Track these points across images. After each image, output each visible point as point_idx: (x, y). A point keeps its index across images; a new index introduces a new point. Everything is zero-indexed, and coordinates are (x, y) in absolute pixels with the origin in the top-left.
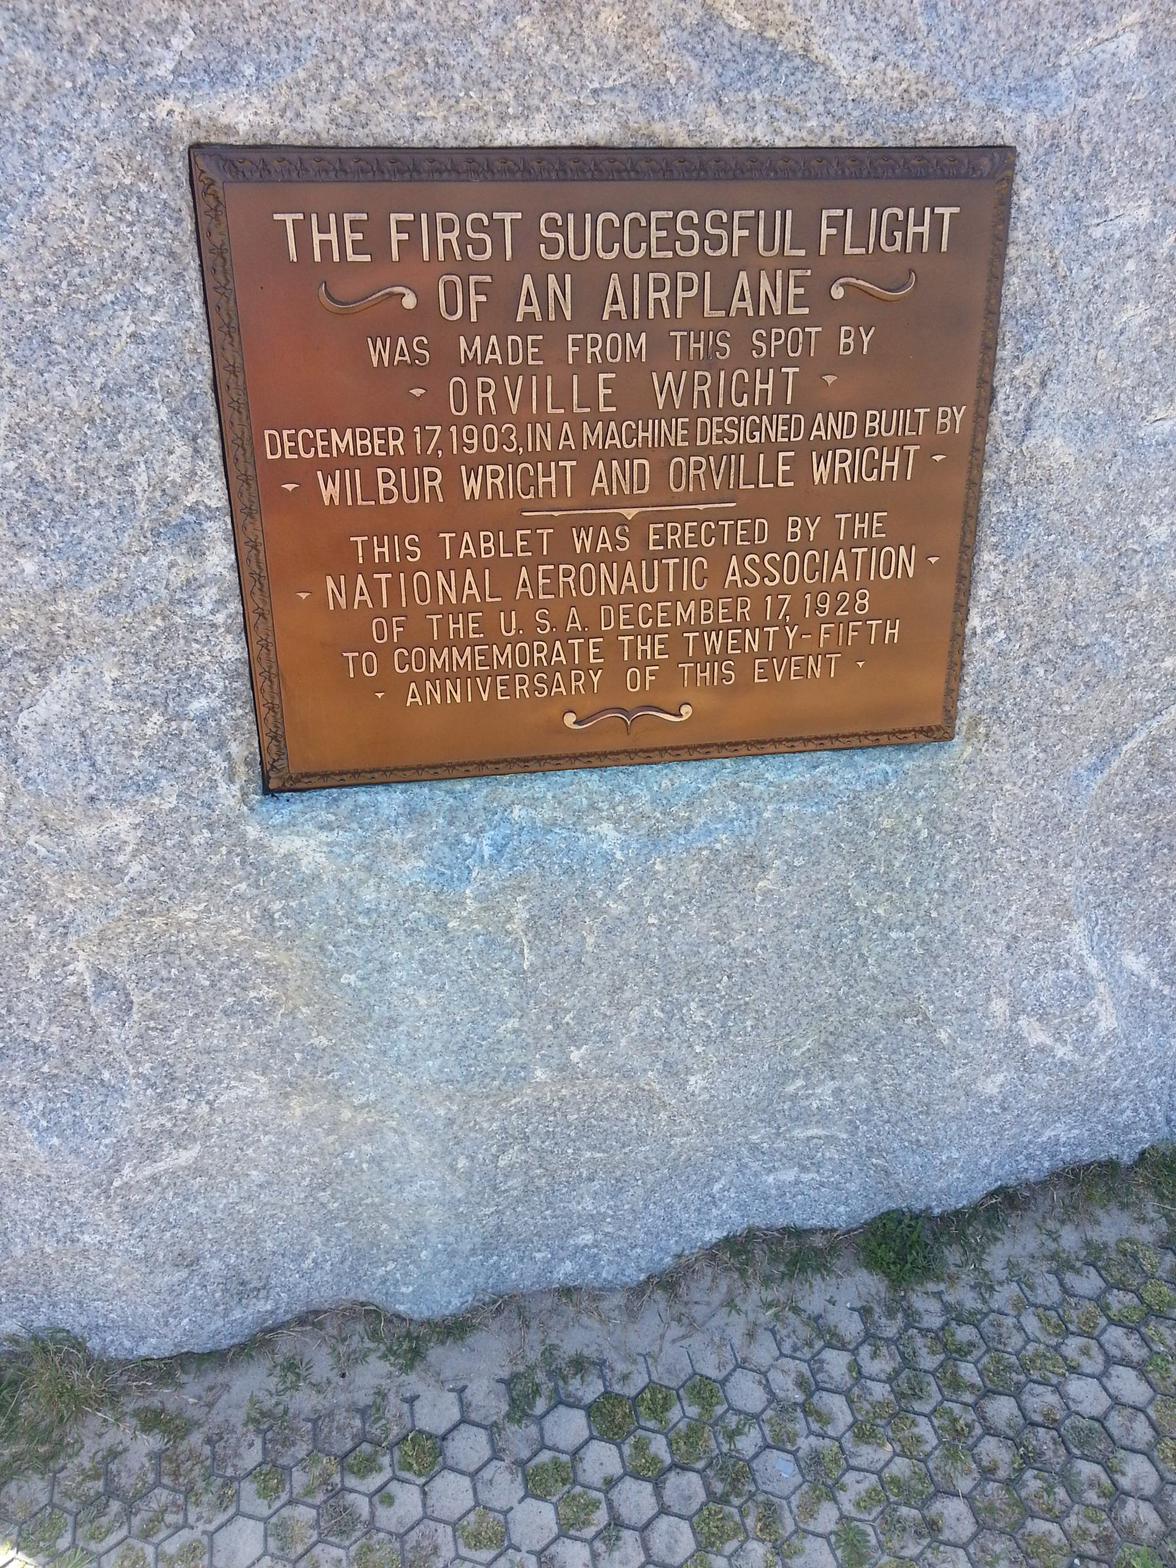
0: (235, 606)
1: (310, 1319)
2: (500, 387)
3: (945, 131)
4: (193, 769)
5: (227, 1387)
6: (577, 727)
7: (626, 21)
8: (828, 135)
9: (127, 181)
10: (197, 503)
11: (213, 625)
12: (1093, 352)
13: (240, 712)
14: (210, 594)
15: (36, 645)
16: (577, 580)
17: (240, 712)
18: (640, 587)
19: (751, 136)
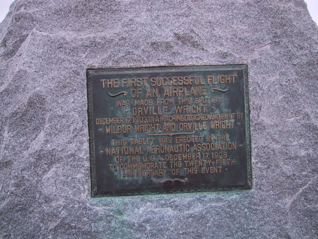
0: (88, 155)
2: (143, 109)
4: (76, 190)
5: (253, 162)
6: (124, 92)
10: (82, 134)
11: (83, 159)
12: (271, 103)
13: (87, 178)
15: (48, 162)
16: (160, 149)
17: (87, 178)
18: (174, 151)
19: (193, 64)
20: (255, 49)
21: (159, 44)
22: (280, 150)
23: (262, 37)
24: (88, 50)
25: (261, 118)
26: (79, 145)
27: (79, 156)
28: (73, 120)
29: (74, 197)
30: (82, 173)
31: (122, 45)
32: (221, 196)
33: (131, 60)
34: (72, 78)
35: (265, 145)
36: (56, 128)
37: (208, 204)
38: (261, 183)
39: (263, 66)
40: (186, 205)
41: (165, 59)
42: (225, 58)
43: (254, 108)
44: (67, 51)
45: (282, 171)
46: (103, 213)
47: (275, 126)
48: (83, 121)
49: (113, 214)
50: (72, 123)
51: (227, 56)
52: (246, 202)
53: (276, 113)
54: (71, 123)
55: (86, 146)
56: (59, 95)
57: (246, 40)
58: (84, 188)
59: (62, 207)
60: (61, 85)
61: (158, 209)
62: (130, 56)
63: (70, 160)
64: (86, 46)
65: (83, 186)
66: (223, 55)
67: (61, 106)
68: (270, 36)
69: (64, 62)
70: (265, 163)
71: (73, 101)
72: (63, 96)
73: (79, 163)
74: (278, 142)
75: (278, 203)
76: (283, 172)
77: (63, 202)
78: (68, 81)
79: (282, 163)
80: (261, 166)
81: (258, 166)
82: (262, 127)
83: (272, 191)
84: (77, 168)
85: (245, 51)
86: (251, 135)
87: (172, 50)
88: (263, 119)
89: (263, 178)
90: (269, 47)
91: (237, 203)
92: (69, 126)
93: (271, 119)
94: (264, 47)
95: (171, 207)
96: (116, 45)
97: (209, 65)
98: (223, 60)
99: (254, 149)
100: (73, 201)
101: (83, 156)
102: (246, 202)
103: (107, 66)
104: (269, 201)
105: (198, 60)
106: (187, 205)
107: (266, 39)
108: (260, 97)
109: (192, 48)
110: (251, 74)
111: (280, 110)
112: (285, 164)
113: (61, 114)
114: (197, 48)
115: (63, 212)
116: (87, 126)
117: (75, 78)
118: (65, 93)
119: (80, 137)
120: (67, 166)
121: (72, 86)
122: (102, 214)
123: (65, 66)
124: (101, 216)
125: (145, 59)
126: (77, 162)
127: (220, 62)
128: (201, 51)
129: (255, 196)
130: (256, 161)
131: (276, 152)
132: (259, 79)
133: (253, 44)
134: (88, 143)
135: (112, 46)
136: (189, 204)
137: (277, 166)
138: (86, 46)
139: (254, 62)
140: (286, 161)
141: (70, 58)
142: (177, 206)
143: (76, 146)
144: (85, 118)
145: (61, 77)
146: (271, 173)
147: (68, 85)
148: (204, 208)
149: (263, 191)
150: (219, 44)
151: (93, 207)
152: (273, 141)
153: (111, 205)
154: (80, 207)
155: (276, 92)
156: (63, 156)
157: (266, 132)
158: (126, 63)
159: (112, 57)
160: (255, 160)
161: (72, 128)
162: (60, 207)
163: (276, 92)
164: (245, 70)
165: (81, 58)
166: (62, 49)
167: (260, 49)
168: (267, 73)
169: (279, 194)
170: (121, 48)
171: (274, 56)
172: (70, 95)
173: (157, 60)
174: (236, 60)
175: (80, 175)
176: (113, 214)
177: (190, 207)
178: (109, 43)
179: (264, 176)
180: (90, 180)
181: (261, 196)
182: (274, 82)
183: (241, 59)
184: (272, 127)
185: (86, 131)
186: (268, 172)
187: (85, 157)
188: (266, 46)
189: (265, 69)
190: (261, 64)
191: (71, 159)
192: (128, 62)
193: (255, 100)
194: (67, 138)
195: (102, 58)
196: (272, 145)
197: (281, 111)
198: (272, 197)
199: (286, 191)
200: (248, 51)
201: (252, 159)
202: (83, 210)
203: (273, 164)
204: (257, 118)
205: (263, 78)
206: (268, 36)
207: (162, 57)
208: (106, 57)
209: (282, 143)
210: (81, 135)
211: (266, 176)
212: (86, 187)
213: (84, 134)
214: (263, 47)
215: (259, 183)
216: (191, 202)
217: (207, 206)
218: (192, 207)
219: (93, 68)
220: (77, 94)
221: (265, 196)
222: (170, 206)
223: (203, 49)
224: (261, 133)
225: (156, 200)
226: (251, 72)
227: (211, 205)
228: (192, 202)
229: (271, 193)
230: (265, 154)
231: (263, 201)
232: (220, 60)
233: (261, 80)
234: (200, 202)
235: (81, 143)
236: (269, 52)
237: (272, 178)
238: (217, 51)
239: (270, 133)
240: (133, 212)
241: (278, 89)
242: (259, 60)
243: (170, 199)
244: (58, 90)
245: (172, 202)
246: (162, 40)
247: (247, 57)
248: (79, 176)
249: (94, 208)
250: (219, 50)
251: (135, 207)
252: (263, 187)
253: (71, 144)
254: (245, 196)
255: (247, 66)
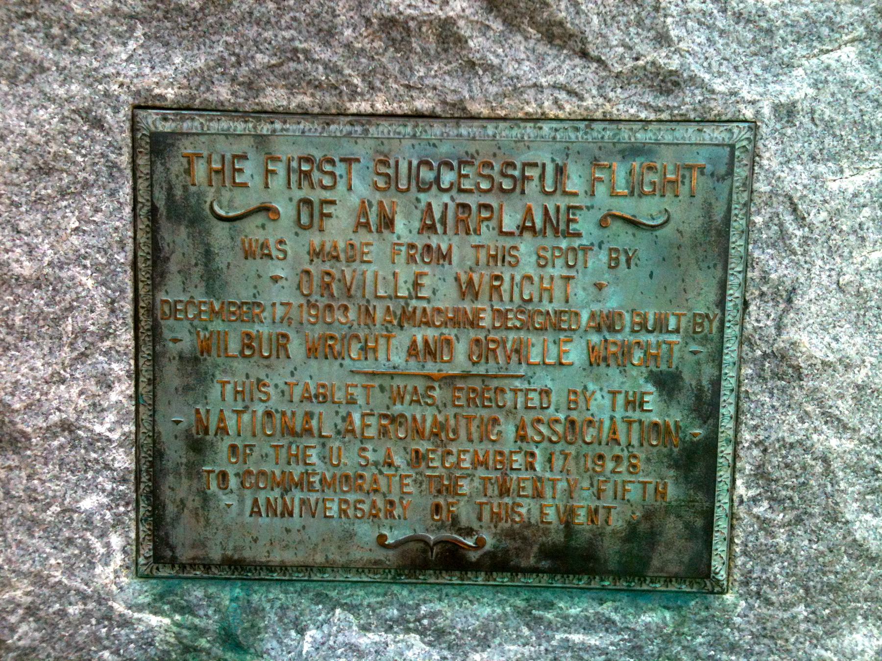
1: (838, 420)
3: (695, 110)
4: (77, 552)
7: (441, 33)
8: (601, 110)
9: (85, 128)
10: (111, 348)
11: (109, 440)
13: (122, 509)
14: (110, 417)
17: (122, 509)
20: (796, 62)
21: (412, 24)
22: (851, 458)
23: (830, 14)
24: (139, 33)
25: (791, 334)
26: (93, 388)
27: (92, 431)
28: (75, 296)
29: (69, 578)
30: (104, 491)
31: (269, 22)
32: (607, 609)
33: (304, 84)
34: (74, 139)
35: (792, 439)
36: (10, 322)
37: (558, 636)
38: (764, 577)
39: (819, 129)
40: (475, 630)
41: (435, 88)
42: (669, 92)
43: (762, 294)
44: (55, 31)
45: (850, 539)
46: (172, 640)
47: (840, 368)
48: (113, 302)
49: (208, 645)
50: (71, 309)
51: (676, 84)
52: (700, 640)
53: (852, 317)
54: (66, 309)
55: (121, 393)
56: (24, 200)
57: (764, 24)
58: (108, 545)
59: (21, 612)
60: (29, 164)
61: (373, 637)
62: (300, 67)
63: (56, 443)
64: (131, 17)
65: (105, 540)
66: (663, 81)
67: (28, 244)
68: (865, 11)
69: (41, 73)
70: (788, 503)
71: (77, 224)
72: (39, 206)
73: (94, 455)
74: (845, 427)
75: (823, 652)
76: (855, 540)
77: (27, 594)
78: (53, 148)
79: (855, 506)
80: (769, 515)
81: (755, 510)
82: (790, 371)
83: (802, 607)
84: (86, 472)
85: (756, 69)
86: (742, 395)
87: (464, 52)
88: (796, 338)
89: (774, 557)
90: (853, 56)
91: (667, 640)
92: (57, 321)
93: (827, 339)
94: (834, 55)
95: (422, 633)
96: (244, 18)
97: (601, 117)
98: (660, 102)
99: (749, 448)
100: (62, 593)
101: (110, 430)
102: (700, 640)
103: (211, 98)
104: (787, 640)
105: (562, 96)
106: (479, 633)
107: (846, 20)
108: (795, 254)
109: (541, 48)
110: (765, 162)
111: (869, 304)
112: (865, 510)
113: (26, 273)
114: (562, 48)
115: (23, 628)
116: (130, 321)
117: (84, 139)
118: (43, 192)
119: (101, 358)
120: (46, 464)
121: (72, 168)
122: (168, 643)
123: (48, 90)
124: (166, 647)
125: (357, 81)
126: (83, 451)
127: (647, 106)
128: (577, 61)
129: (737, 620)
130: (752, 493)
131: (836, 465)
132: (795, 178)
133: (790, 38)
134: (133, 383)
135: (229, 24)
136: (484, 627)
137: (833, 517)
138: (131, 17)
139: (787, 112)
140: (868, 497)
141: (65, 60)
142: (440, 633)
143: (81, 393)
144: (122, 291)
145: (31, 131)
146: (806, 542)
147: (60, 165)
148: (542, 648)
149: (768, 602)
150: (651, 34)
151: (137, 615)
152: (826, 423)
153: (202, 613)
154: (86, 615)
155: (861, 233)
156: (29, 430)
157: (801, 387)
158: (283, 91)
159: (228, 65)
160: (748, 487)
161: (69, 326)
162: (13, 612)
163: (861, 233)
164: (745, 143)
165: (110, 61)
166: (33, 23)
167: (814, 61)
168: (834, 157)
169: (829, 619)
170: (266, 35)
171: (870, 93)
172: (65, 203)
173: (402, 90)
174: (713, 104)
175: (94, 497)
176: (208, 645)
177: (489, 637)
178: (219, 9)
179: (777, 552)
180: (132, 515)
181: (760, 620)
182: (855, 195)
183: (733, 98)
184: (830, 371)
185: (126, 338)
186: (796, 539)
187: (115, 436)
188: (840, 47)
189: (826, 141)
190: (813, 119)
191: (62, 439)
192: (291, 89)
193: (771, 263)
194: (49, 364)
195: (190, 66)
196: (822, 437)
197: (871, 308)
198: (803, 627)
199: (856, 609)
200: (765, 69)
201: (739, 482)
202: (98, 623)
203: (817, 510)
204: (773, 331)
205: (816, 178)
206: (856, 9)
207: (421, 78)
208: (207, 65)
209: (863, 432)
210: (105, 353)
211: (786, 553)
212: (116, 540)
213: (118, 352)
214: (828, 51)
215: (755, 576)
216: (494, 620)
217: (554, 643)
218: (497, 641)
219: (157, 103)
220: (93, 200)
221: (776, 622)
222: (416, 631)
223: (584, 54)
224: (783, 390)
225: (369, 605)
226: (767, 155)
227: (567, 640)
228: (500, 624)
229: (800, 613)
230: (789, 472)
231: (766, 641)
232: (649, 98)
233: (805, 187)
234: (527, 625)
235: (105, 382)
236: (850, 74)
237: (808, 558)
238: (641, 63)
239: (819, 395)
240: (280, 643)
241: (871, 224)
242: (806, 104)
243: (418, 605)
244: (17, 181)
245: (425, 617)
246: (425, 11)
247: (761, 90)
248: (88, 503)
249: (140, 620)
250: (649, 58)
251: (291, 626)
252: (768, 591)
253: (62, 387)
254: (698, 617)
255: (757, 127)
